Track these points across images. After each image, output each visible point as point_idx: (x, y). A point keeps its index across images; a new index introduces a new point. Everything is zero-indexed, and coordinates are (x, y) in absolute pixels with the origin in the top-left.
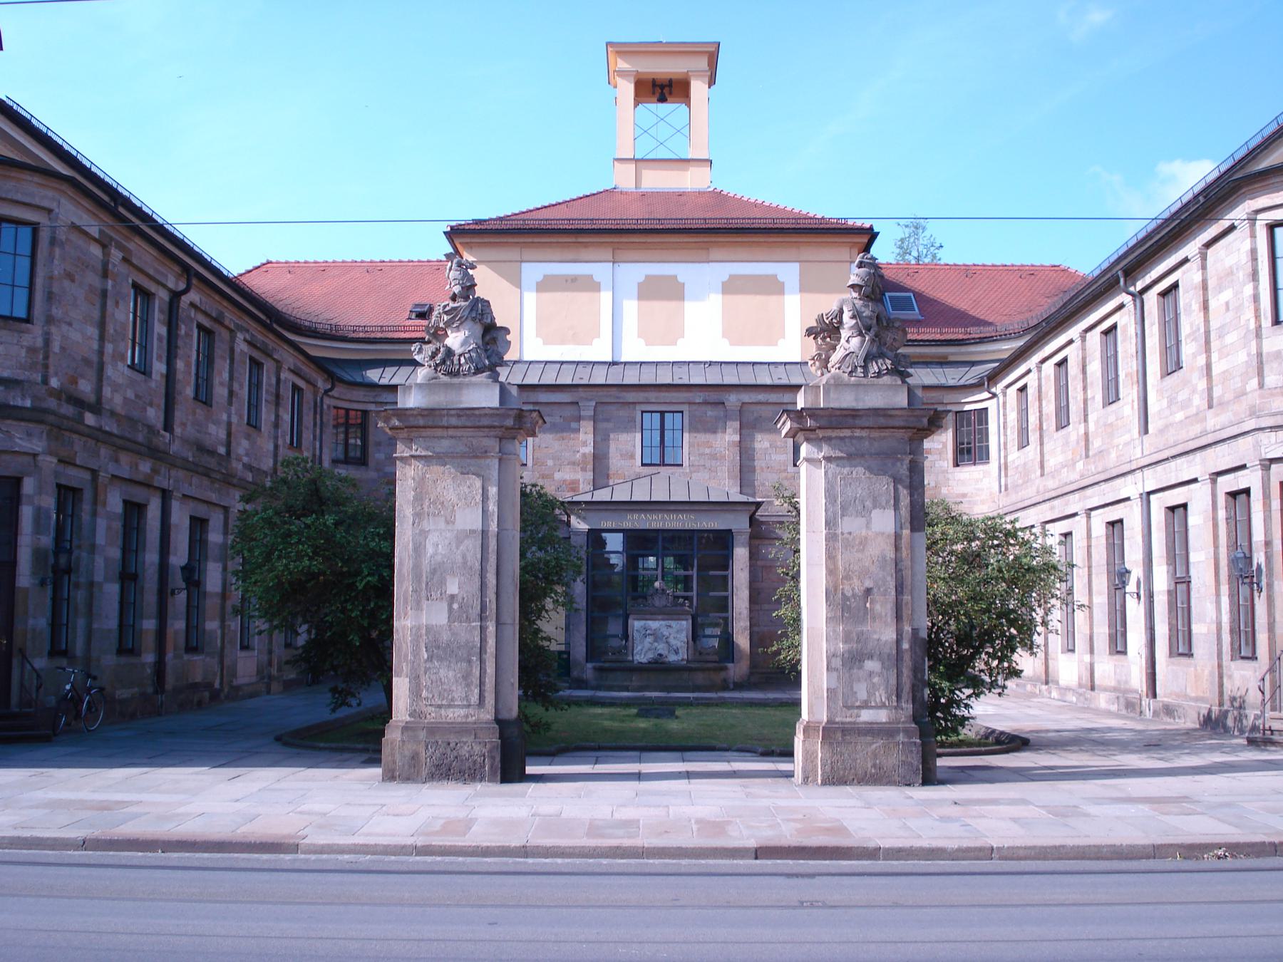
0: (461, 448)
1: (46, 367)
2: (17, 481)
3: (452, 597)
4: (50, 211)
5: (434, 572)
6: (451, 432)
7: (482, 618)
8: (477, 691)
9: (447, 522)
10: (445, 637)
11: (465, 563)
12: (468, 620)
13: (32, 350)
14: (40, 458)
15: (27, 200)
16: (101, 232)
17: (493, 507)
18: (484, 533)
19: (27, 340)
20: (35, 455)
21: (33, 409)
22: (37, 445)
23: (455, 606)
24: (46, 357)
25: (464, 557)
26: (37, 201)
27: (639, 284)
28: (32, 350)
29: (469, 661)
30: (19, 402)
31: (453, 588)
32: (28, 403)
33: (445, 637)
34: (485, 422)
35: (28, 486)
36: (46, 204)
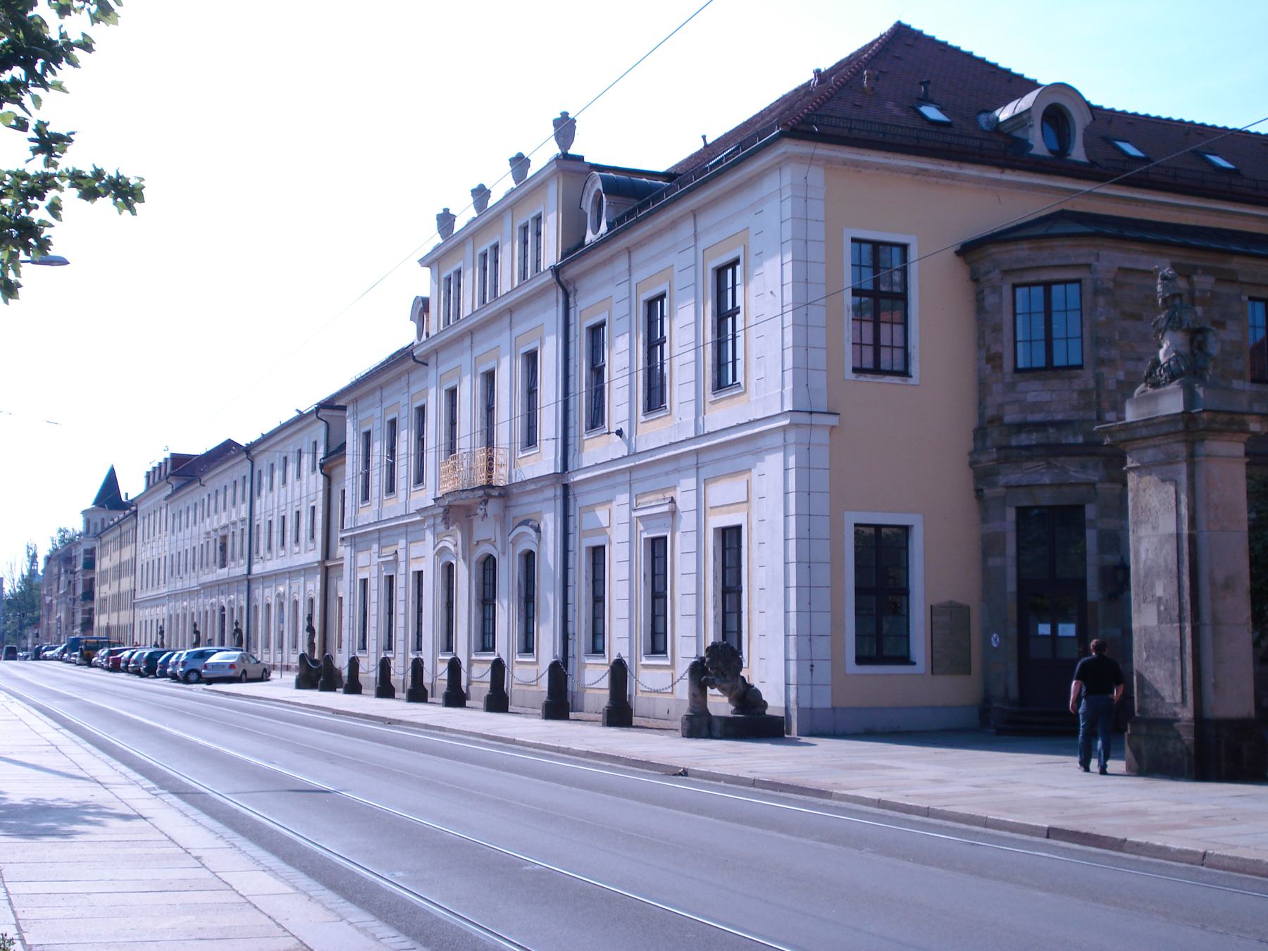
0: (1161, 457)
1: (1099, 404)
2: (1079, 509)
3: (1160, 599)
4: (1089, 266)
5: (1146, 576)
6: (1151, 442)
7: (1181, 620)
8: (1179, 690)
9: (1154, 528)
10: (1157, 637)
11: (1166, 566)
12: (1171, 621)
13: (1083, 393)
14: (1098, 486)
15: (1064, 262)
16: (1174, 266)
17: (1184, 511)
18: (1178, 536)
19: (1078, 384)
20: (1094, 484)
21: (1086, 444)
22: (1093, 476)
23: (1162, 608)
24: (1098, 396)
25: (1166, 560)
26: (1073, 261)
27: (85, 512)
28: (1083, 393)
29: (1173, 661)
30: (1071, 440)
31: (1159, 592)
32: (1080, 440)
33: (1157, 637)
34: (1165, 429)
35: (1090, 512)
36: (1082, 261)
